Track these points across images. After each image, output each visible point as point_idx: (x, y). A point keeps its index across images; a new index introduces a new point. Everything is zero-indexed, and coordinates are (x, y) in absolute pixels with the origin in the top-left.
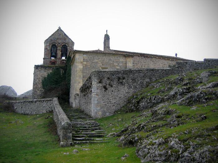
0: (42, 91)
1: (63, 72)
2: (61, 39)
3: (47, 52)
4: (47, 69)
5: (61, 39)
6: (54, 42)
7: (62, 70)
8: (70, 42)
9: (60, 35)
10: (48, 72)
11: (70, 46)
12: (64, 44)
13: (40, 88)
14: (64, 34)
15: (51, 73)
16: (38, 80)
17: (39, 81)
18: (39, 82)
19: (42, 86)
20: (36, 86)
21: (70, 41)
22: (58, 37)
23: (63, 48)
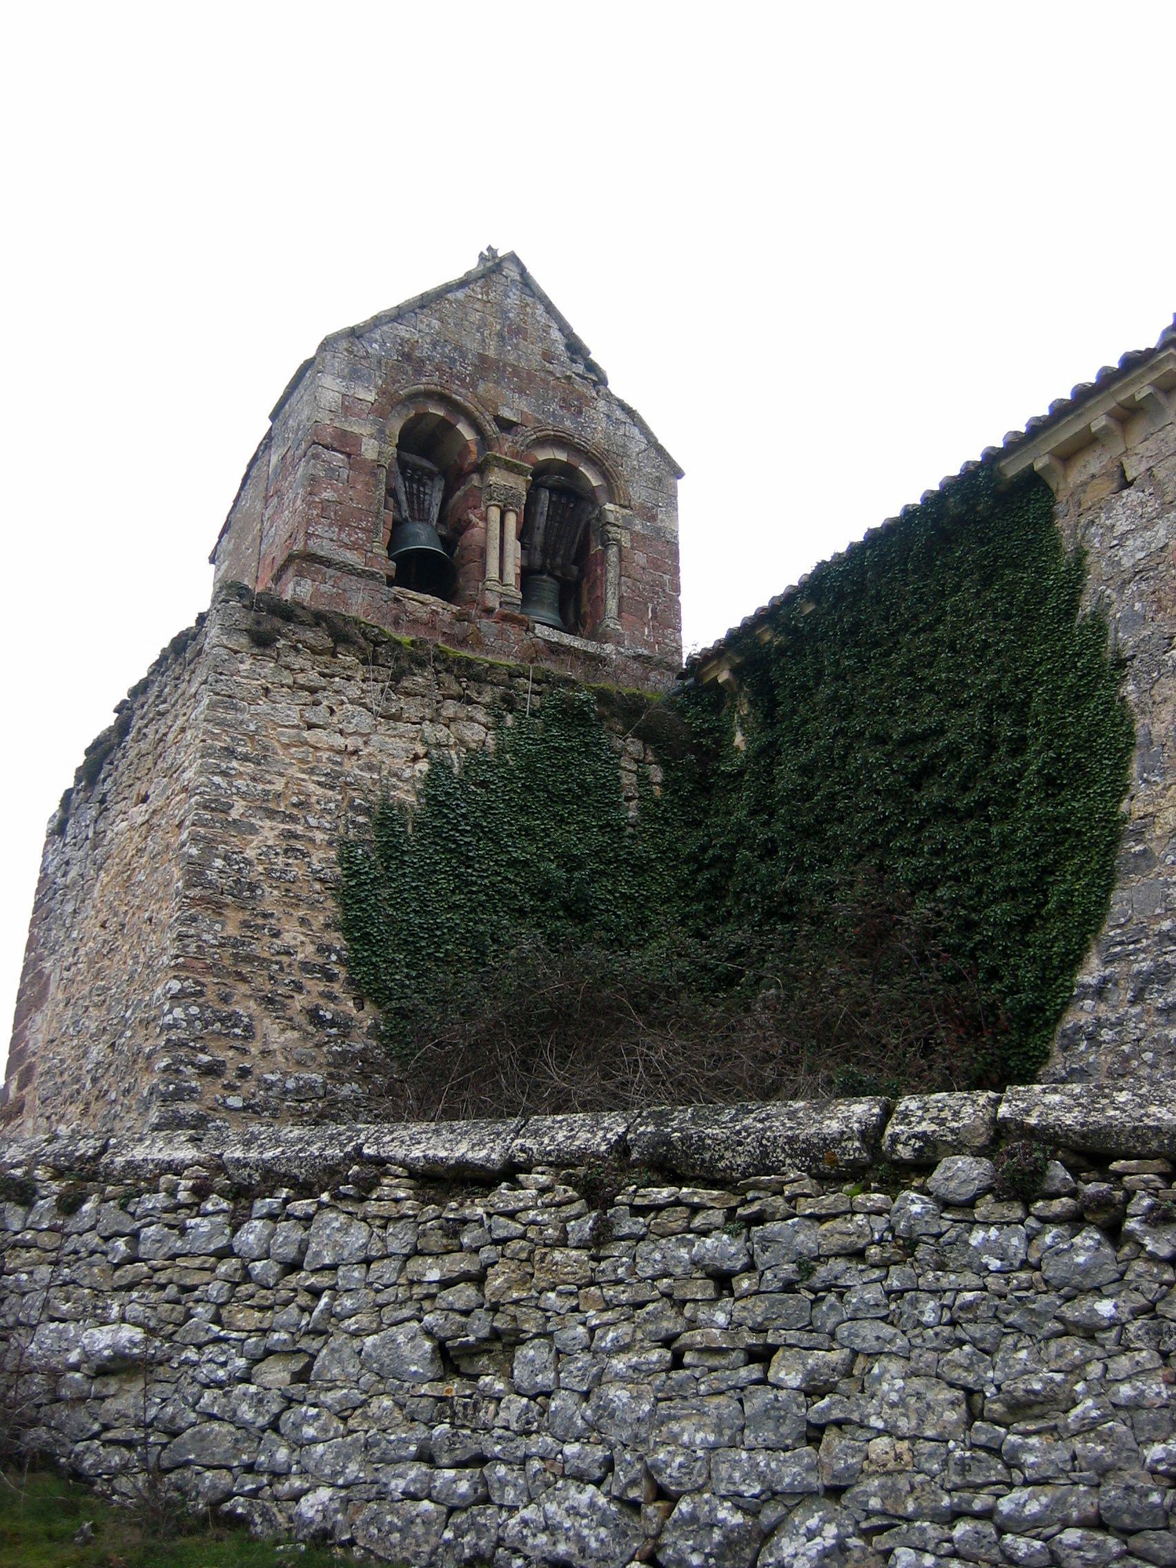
0: (344, 1026)
1: (644, 779)
2: (524, 381)
3: (350, 484)
4: (419, 680)
5: (524, 381)
6: (443, 399)
7: (635, 747)
8: (634, 449)
9: (519, 331)
10: (441, 733)
11: (638, 493)
12: (562, 456)
13: (315, 986)
14: (556, 334)
15: (475, 758)
16: (269, 831)
17: (292, 845)
18: (297, 869)
19: (336, 940)
20: (232, 930)
21: (638, 444)
22: (491, 353)
23: (545, 495)
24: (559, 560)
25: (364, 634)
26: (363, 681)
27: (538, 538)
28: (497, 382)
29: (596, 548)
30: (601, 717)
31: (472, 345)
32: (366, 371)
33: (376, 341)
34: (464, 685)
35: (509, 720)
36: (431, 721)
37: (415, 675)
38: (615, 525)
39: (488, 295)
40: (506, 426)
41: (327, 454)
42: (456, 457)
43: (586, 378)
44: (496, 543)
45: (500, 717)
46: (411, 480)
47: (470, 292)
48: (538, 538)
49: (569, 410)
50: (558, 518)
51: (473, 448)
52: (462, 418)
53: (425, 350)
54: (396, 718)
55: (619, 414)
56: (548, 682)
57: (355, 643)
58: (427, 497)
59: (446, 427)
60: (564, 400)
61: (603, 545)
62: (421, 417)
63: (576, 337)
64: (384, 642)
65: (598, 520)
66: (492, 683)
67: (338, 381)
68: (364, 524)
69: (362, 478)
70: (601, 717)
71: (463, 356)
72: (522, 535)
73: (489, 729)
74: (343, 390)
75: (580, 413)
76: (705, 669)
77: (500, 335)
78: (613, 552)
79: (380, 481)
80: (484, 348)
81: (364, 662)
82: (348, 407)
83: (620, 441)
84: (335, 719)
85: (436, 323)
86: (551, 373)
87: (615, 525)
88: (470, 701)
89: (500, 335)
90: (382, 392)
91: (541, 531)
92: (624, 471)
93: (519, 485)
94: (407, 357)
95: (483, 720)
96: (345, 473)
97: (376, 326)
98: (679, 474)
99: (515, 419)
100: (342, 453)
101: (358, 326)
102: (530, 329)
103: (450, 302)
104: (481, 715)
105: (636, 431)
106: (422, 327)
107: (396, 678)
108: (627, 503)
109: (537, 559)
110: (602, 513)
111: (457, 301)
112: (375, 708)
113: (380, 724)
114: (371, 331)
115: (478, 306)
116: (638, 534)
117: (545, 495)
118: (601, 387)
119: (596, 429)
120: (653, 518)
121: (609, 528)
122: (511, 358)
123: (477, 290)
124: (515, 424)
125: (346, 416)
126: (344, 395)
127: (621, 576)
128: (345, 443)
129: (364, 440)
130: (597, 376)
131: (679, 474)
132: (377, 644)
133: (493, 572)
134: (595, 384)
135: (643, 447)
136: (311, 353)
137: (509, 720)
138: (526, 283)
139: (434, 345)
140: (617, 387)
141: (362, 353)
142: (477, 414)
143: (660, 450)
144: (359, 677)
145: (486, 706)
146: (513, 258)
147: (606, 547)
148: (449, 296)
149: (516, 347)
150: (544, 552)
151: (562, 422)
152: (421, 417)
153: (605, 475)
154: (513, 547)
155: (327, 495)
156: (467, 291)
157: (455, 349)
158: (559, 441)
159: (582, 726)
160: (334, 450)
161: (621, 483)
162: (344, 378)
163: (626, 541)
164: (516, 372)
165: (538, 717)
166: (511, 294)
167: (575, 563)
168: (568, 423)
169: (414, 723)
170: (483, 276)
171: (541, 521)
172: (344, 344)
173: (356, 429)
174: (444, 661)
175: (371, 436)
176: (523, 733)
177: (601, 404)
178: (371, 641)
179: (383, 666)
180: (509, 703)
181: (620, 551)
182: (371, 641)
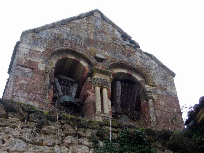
2: (105, 46)
5: (105, 46)
6: (73, 52)
8: (153, 67)
12: (125, 71)
14: (116, 32)
21: (154, 65)
22: (92, 37)
23: (119, 83)
24: (129, 109)
25: (23, 110)
26: (22, 128)
27: (118, 101)
28: (95, 46)
29: (143, 102)
30: (150, 141)
31: (84, 35)
32: (40, 43)
33: (44, 34)
34: (76, 129)
35: (101, 144)
36: (59, 145)
37: (50, 125)
38: (150, 92)
39: (89, 21)
40: (100, 60)
41: (22, 69)
42: (81, 75)
43: (130, 46)
44: (99, 99)
45: (96, 143)
46: (64, 85)
47: (81, 21)
48: (118, 101)
49: (125, 55)
50: (126, 92)
51: (87, 69)
52: (82, 59)
53: (65, 36)
54: (40, 144)
55: (145, 56)
56: (121, 127)
57: (18, 112)
58: (71, 90)
59: (76, 63)
60: (123, 52)
61: (146, 100)
62: (65, 60)
63: (125, 33)
64: (33, 112)
65: (143, 92)
66: (91, 128)
67: (28, 45)
68: (39, 92)
69: (38, 76)
70: (150, 141)
71: (80, 39)
72: (112, 98)
73: (90, 148)
74: (30, 48)
75: (130, 56)
76: (198, 115)
77: (95, 33)
78: (150, 102)
79: (46, 78)
80: (89, 36)
81: (23, 120)
82: (32, 53)
83: (148, 65)
84: (5, 145)
85: (69, 29)
86: (116, 44)
87: (150, 92)
88: (80, 136)
89: (95, 33)
90: (46, 49)
91: (119, 97)
92: (151, 74)
93: (108, 79)
94: (58, 39)
95: (87, 144)
96: (30, 75)
97: (44, 30)
98: (173, 75)
99: (103, 58)
100: (29, 68)
101: (36, 29)
102: (106, 31)
103: (74, 23)
104: (85, 142)
105: (153, 62)
106: (64, 30)
107: (40, 127)
108: (153, 84)
109: (119, 109)
110: (144, 89)
111: (76, 23)
112: (27, 139)
113: (30, 147)
114: (42, 31)
115: (85, 24)
116: (160, 95)
117: (119, 83)
118: (137, 49)
119: (137, 61)
120: (166, 89)
121: (147, 93)
122: (100, 39)
123: (85, 20)
124: (104, 59)
125: (31, 56)
126: (30, 50)
127: (155, 109)
128: (32, 66)
129: (39, 64)
130: (135, 45)
131: (173, 75)
132: (30, 112)
133: (99, 108)
134: (134, 48)
135: (157, 66)
136: (18, 40)
137: (101, 144)
138: (103, 18)
139: (68, 35)
140: (144, 48)
141: (38, 37)
142: (87, 56)
143: (164, 67)
144: (19, 126)
145: (89, 138)
146: (97, 11)
147: (147, 100)
148: (74, 21)
149: (102, 36)
150: (122, 106)
151: (123, 58)
152: (65, 60)
153: (143, 76)
154: (108, 103)
155: (23, 82)
156: (81, 20)
157: (77, 37)
158: (122, 65)
159: (140, 145)
160: (26, 67)
161: (150, 78)
162: (30, 44)
163: (155, 97)
164: (102, 43)
165: (117, 142)
166: (98, 21)
167: (136, 110)
168: (125, 59)
169: (49, 146)
170: (87, 16)
171: (119, 93)
172: (31, 35)
173: (36, 60)
174: (66, 120)
175: (42, 63)
176: (109, 148)
177: (138, 53)
178: (27, 111)
179: (33, 121)
180: (101, 136)
181: (153, 101)
182: (27, 111)
